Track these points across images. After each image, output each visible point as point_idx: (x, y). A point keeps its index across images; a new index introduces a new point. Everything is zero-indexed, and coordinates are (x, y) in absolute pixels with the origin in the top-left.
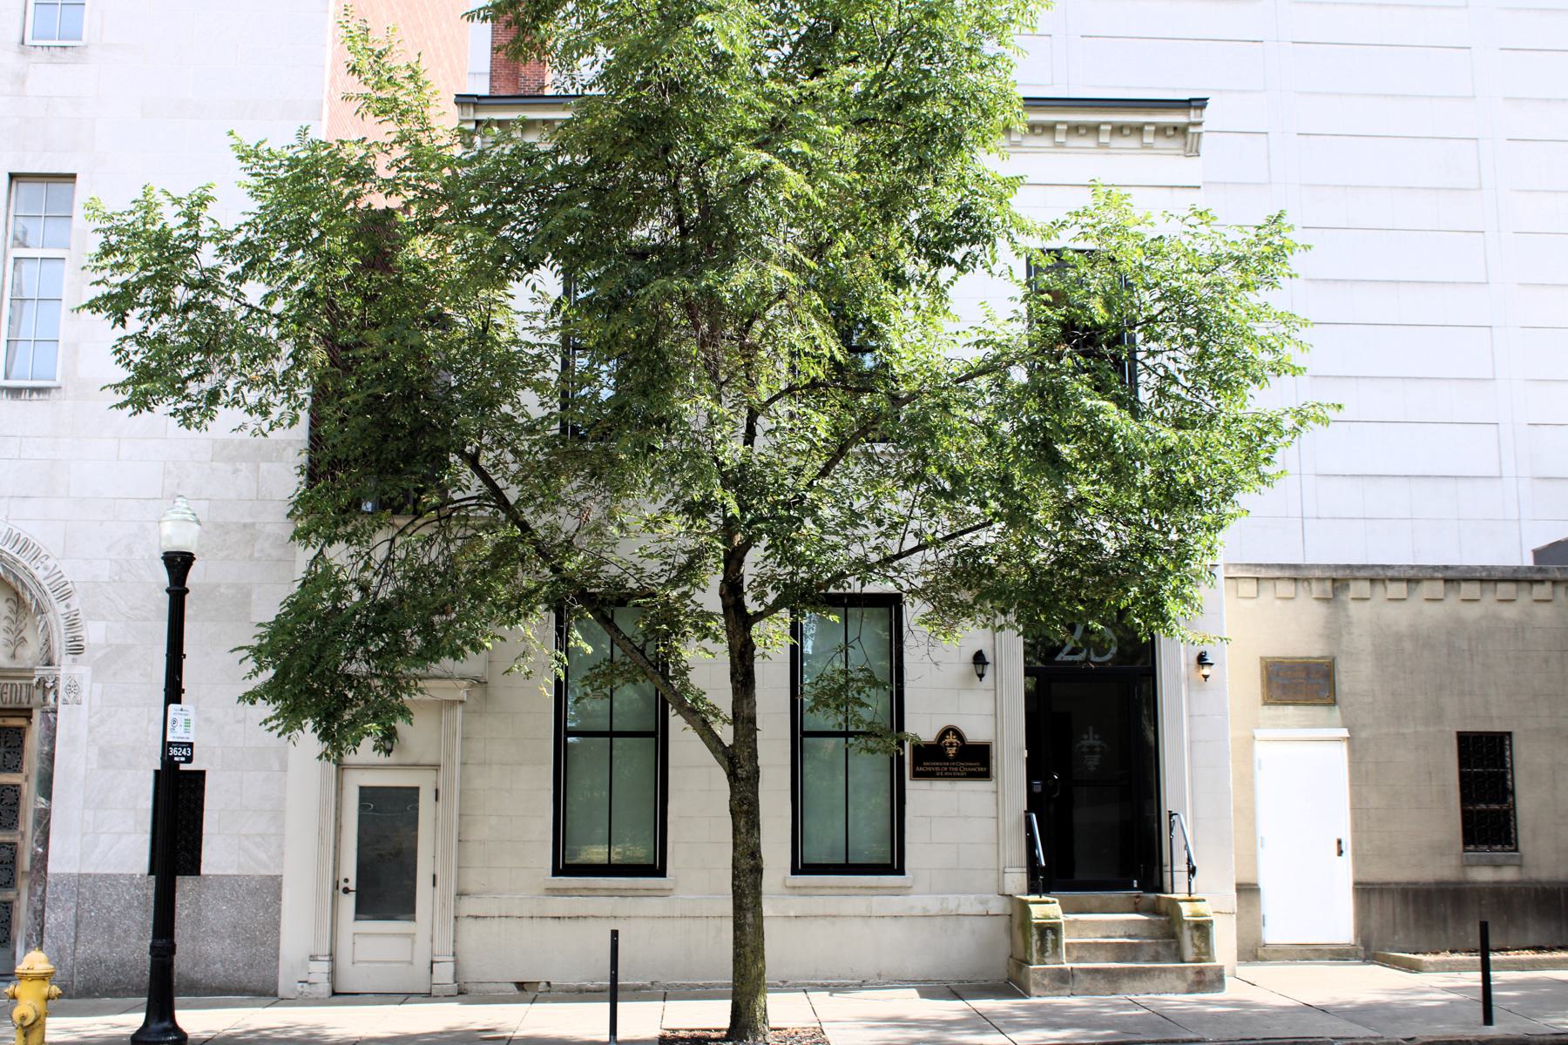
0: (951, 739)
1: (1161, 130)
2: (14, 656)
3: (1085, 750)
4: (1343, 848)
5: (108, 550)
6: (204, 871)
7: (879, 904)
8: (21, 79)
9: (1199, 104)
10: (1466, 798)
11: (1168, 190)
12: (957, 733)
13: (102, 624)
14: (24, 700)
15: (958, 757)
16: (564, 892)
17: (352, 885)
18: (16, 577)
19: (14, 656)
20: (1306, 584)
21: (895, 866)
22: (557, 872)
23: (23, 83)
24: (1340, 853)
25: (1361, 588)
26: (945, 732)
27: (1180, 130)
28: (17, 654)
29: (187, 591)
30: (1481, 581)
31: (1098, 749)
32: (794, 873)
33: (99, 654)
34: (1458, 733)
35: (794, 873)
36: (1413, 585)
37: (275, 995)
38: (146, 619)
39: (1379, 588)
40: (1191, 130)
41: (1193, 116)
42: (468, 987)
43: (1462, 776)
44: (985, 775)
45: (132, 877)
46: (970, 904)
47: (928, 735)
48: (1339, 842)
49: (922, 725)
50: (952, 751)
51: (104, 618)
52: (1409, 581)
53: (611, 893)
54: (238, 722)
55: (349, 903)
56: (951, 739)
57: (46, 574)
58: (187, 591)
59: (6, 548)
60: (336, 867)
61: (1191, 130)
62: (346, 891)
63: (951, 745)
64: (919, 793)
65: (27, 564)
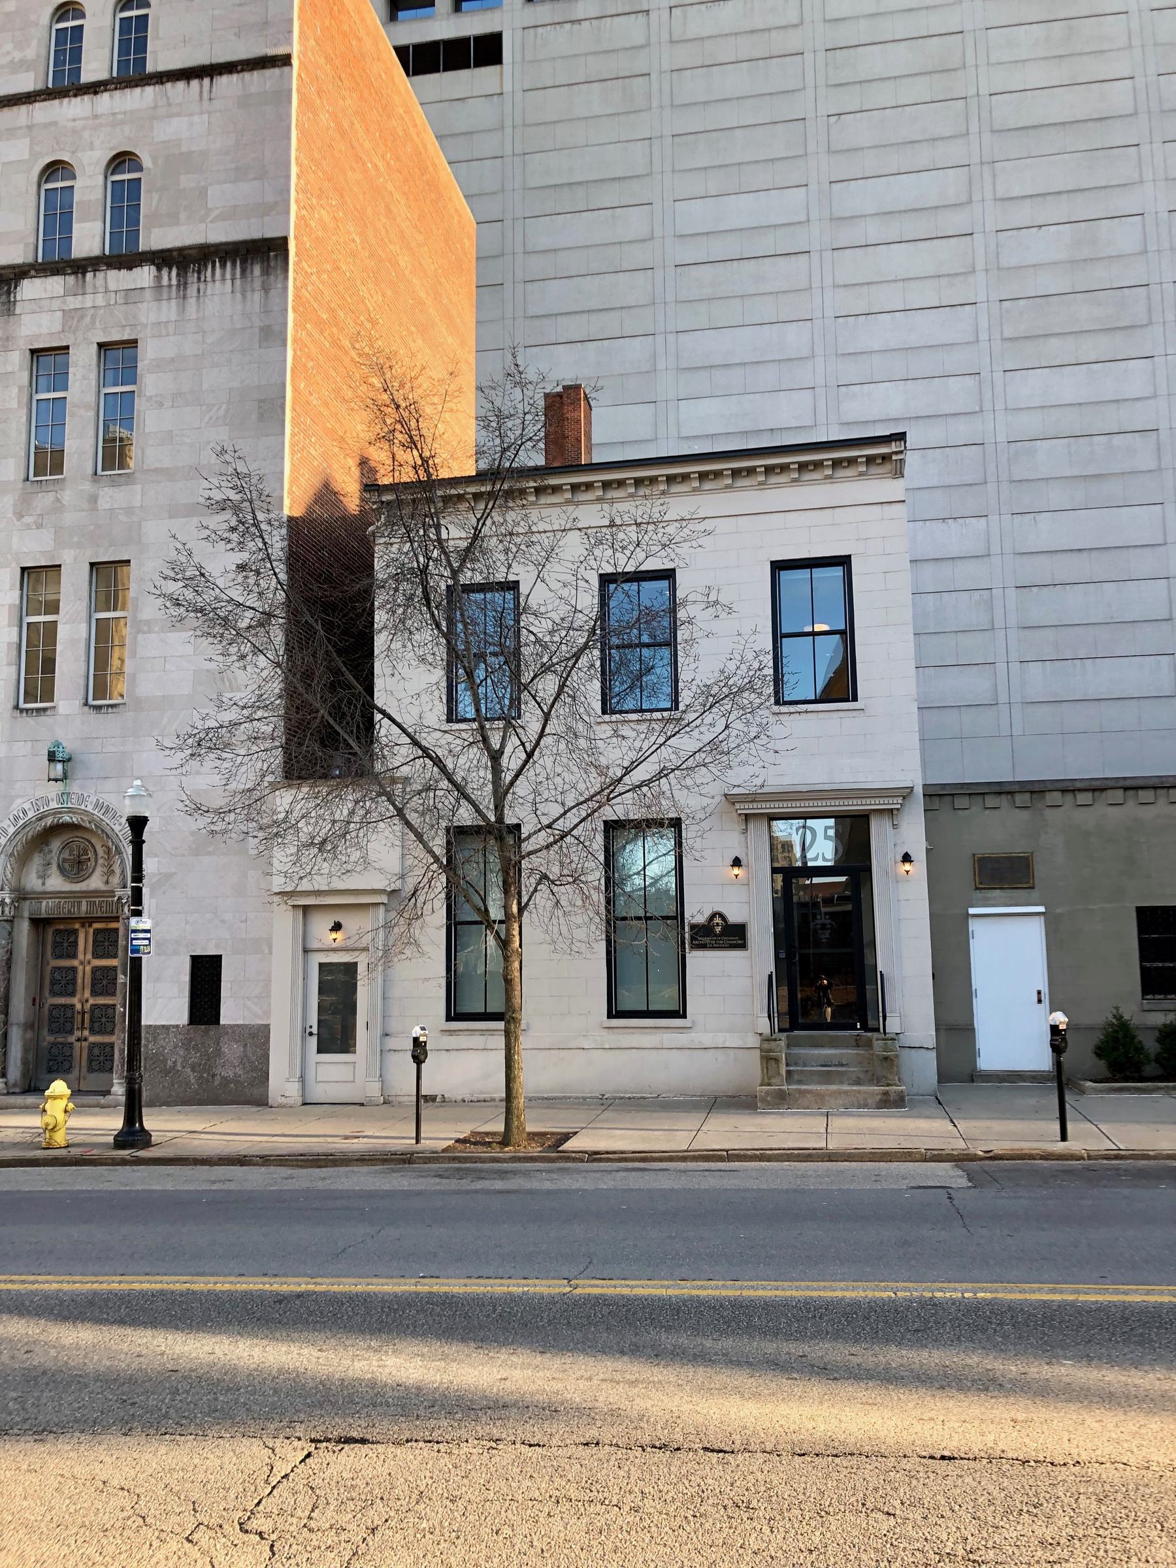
0: (717, 920)
1: (870, 460)
2: (107, 882)
3: (819, 927)
4: (1043, 999)
5: (158, 810)
6: (222, 1022)
7: (670, 1038)
8: (94, 499)
9: (901, 437)
10: (1144, 957)
11: (880, 506)
12: (722, 916)
13: (156, 859)
14: (115, 911)
15: (722, 933)
16: (450, 1032)
17: (315, 1030)
18: (103, 831)
19: (107, 882)
20: (1009, 797)
21: (680, 1013)
22: (449, 1018)
23: (96, 501)
24: (1040, 1001)
25: (1056, 797)
26: (713, 916)
27: (885, 458)
28: (110, 881)
29: (144, 842)
30: (1155, 788)
31: (829, 926)
32: (609, 1017)
33: (154, 880)
34: (1137, 908)
35: (609, 1017)
36: (1097, 794)
37: (267, 1104)
38: (183, 855)
39: (1069, 796)
40: (894, 457)
41: (894, 447)
42: (390, 1099)
43: (1141, 942)
44: (743, 946)
45: (177, 1026)
46: (733, 1041)
47: (701, 919)
48: (1039, 993)
49: (696, 912)
50: (718, 929)
51: (156, 856)
52: (1094, 790)
53: (482, 1032)
54: (242, 922)
55: (313, 1041)
56: (717, 920)
57: (120, 828)
58: (144, 842)
59: (95, 812)
60: (305, 1018)
61: (894, 457)
62: (311, 1034)
63: (718, 925)
64: (697, 961)
65: (108, 822)
